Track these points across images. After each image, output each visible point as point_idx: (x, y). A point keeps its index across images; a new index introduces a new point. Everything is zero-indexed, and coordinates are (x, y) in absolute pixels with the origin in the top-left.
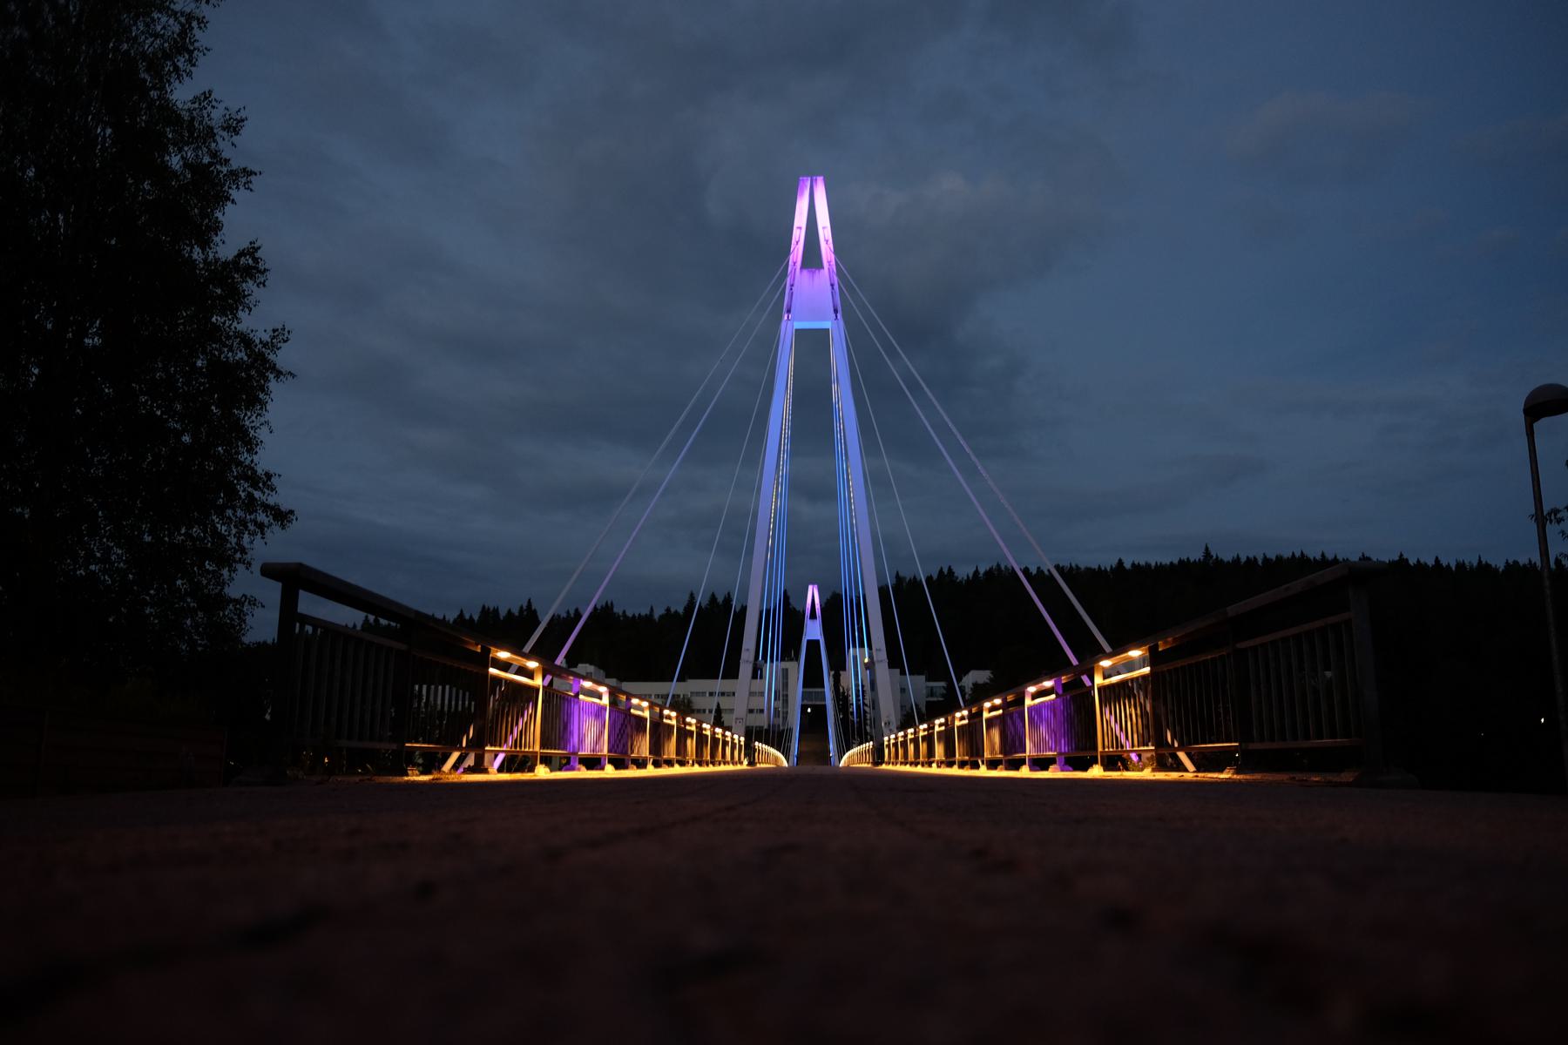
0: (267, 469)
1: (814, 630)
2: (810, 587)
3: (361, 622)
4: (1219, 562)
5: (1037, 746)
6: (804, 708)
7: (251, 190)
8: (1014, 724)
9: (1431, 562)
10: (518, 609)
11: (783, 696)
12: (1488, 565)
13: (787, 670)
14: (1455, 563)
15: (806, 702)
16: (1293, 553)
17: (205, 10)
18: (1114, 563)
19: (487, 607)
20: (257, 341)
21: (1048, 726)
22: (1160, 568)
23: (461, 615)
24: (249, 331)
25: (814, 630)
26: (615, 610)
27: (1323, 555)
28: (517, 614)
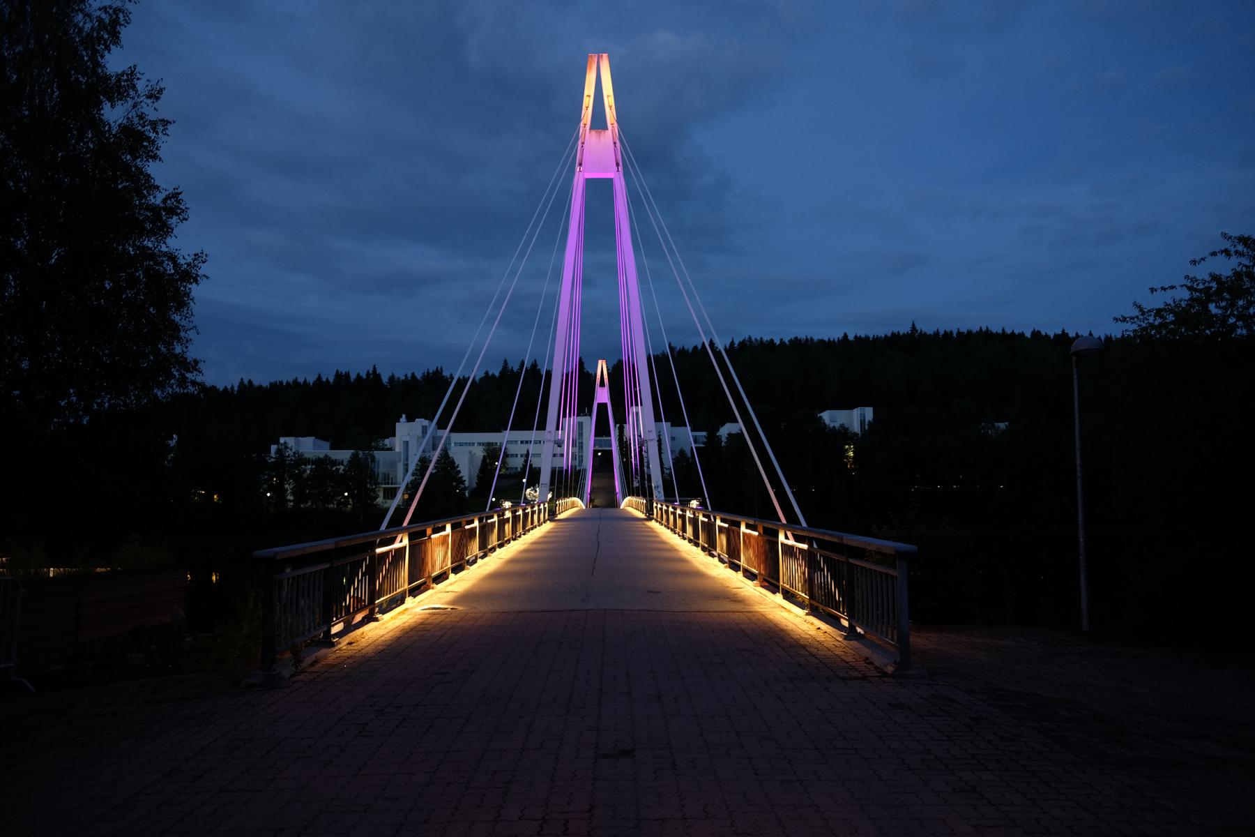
0: (194, 357)
1: (602, 395)
2: (600, 362)
3: (238, 384)
4: (923, 335)
5: (748, 561)
6: (595, 452)
7: (168, 135)
8: (734, 538)
10: (366, 372)
11: (578, 444)
13: (582, 423)
15: (597, 448)
16: (981, 328)
17: (129, 6)
18: (841, 336)
19: (340, 372)
21: (754, 551)
22: (876, 340)
23: (319, 378)
24: (175, 251)
25: (602, 395)
26: (444, 374)
27: (1003, 330)
28: (364, 377)
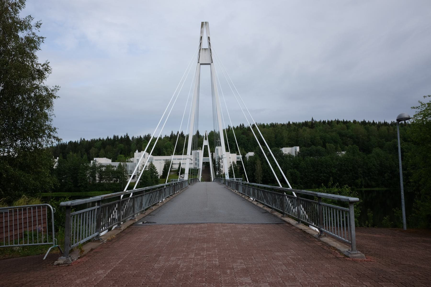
4: (315, 122)
7: (49, 63)
9: (372, 122)
12: (386, 122)
14: (378, 122)
18: (288, 122)
20: (50, 90)
